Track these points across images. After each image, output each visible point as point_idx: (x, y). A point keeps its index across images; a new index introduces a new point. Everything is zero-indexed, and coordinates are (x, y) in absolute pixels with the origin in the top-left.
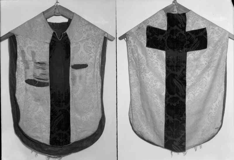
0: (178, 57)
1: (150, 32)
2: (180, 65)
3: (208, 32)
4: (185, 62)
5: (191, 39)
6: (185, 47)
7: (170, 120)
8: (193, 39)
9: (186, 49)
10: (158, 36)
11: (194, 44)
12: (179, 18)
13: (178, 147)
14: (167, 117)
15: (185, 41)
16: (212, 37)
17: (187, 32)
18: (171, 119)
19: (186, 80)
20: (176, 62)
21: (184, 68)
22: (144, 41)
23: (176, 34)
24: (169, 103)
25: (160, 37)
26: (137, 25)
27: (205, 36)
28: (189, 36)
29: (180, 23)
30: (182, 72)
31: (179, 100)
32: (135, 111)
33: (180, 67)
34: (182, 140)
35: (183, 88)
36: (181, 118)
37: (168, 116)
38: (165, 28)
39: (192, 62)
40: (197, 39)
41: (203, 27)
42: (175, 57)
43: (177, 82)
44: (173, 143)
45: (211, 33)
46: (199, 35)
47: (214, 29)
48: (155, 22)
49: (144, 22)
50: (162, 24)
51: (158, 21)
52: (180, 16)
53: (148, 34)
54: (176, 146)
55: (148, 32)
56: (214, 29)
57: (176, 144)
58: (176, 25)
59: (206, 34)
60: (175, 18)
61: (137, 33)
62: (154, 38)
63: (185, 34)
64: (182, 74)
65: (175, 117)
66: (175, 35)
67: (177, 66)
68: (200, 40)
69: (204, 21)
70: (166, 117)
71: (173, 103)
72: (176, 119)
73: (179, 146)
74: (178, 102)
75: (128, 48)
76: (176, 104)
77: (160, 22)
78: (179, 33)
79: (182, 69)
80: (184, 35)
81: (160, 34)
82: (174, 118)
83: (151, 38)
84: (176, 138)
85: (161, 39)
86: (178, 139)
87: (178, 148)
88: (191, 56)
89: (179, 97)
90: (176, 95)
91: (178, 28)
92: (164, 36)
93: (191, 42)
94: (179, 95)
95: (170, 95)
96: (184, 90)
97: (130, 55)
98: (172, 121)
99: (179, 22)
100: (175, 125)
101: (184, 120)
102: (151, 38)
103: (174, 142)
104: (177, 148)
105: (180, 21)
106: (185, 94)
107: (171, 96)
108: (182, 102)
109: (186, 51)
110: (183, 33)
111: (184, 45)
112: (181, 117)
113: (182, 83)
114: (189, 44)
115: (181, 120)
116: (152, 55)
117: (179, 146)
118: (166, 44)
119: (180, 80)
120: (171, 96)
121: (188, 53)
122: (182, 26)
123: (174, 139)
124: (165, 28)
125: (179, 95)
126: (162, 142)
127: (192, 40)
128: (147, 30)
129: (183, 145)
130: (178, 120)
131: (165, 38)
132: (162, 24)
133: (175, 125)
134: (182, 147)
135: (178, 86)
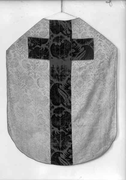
0: (62, 66)
1: (32, 42)
2: (65, 75)
3: (95, 43)
4: (70, 71)
5: (76, 47)
6: (70, 55)
7: (56, 132)
8: (79, 48)
9: (71, 57)
10: (40, 46)
11: (80, 53)
12: (64, 25)
13: (64, 160)
14: (53, 128)
15: (71, 49)
16: (98, 49)
17: (73, 39)
18: (56, 130)
19: (71, 90)
20: (61, 71)
21: (69, 77)
22: (26, 52)
23: (61, 40)
24: (54, 114)
25: (44, 46)
26: (16, 40)
27: (91, 47)
28: (74, 44)
29: (65, 29)
30: (67, 81)
31: (64, 111)
32: (24, 59)
33: (64, 76)
34: (69, 153)
35: (68, 98)
36: (67, 129)
37: (54, 127)
38: (48, 37)
39: (77, 71)
40: (83, 48)
41: (90, 37)
42: (55, 28)
43: (62, 92)
44: (59, 156)
45: (99, 45)
46: (86, 44)
47: (101, 41)
48: (37, 31)
49: (25, 34)
50: (45, 33)
51: (40, 30)
52: (64, 23)
53: (30, 45)
54: (63, 159)
55: (30, 42)
56: (101, 41)
57: (63, 156)
58: (61, 32)
59: (92, 44)
60: (59, 25)
61: (18, 45)
62: (36, 47)
63: (71, 40)
64: (67, 83)
65: (60, 128)
66: (60, 42)
67: (61, 76)
68: (85, 49)
69: (92, 32)
70: (52, 128)
71: (59, 114)
72: (61, 130)
73: (66, 160)
74: (64, 112)
75: (8, 61)
76: (61, 115)
77: (42, 31)
78: (63, 39)
79: (67, 78)
80: (70, 42)
81: (43, 44)
82: (59, 129)
83: (34, 48)
84: (62, 149)
85: (44, 49)
86: (65, 151)
87: (65, 161)
88: (76, 64)
89: (64, 107)
90: (61, 106)
91: (63, 35)
92: (47, 45)
93: (77, 50)
94: (64, 105)
95: (54, 106)
96: (69, 100)
97: (10, 68)
98: (58, 133)
99: (64, 29)
100: (60, 136)
101: (70, 130)
102: (34, 48)
103: (61, 154)
104: (64, 162)
105: (64, 27)
106: (70, 105)
107: (56, 107)
108: (67, 112)
109: (71, 59)
110: (69, 39)
111: (69, 53)
112: (66, 128)
113: (66, 93)
114: (74, 53)
115: (66, 131)
116: (35, 66)
117: (66, 160)
118: (50, 52)
119: (66, 90)
120: (56, 107)
121: (72, 61)
122: (66, 32)
123: (61, 151)
124: (48, 37)
125: (64, 105)
126: (49, 156)
127: (78, 49)
128: (29, 40)
129: (70, 158)
130: (64, 132)
131: (48, 46)
132: (45, 33)
133: (60, 136)
134: (69, 160)
135: (63, 96)
